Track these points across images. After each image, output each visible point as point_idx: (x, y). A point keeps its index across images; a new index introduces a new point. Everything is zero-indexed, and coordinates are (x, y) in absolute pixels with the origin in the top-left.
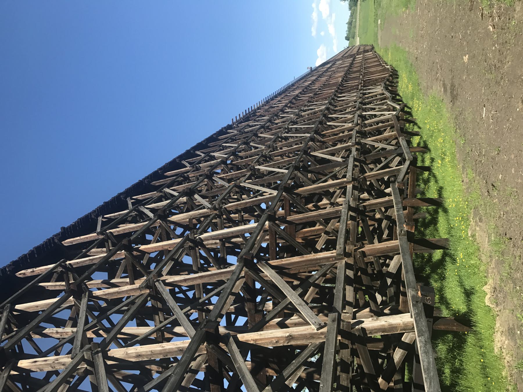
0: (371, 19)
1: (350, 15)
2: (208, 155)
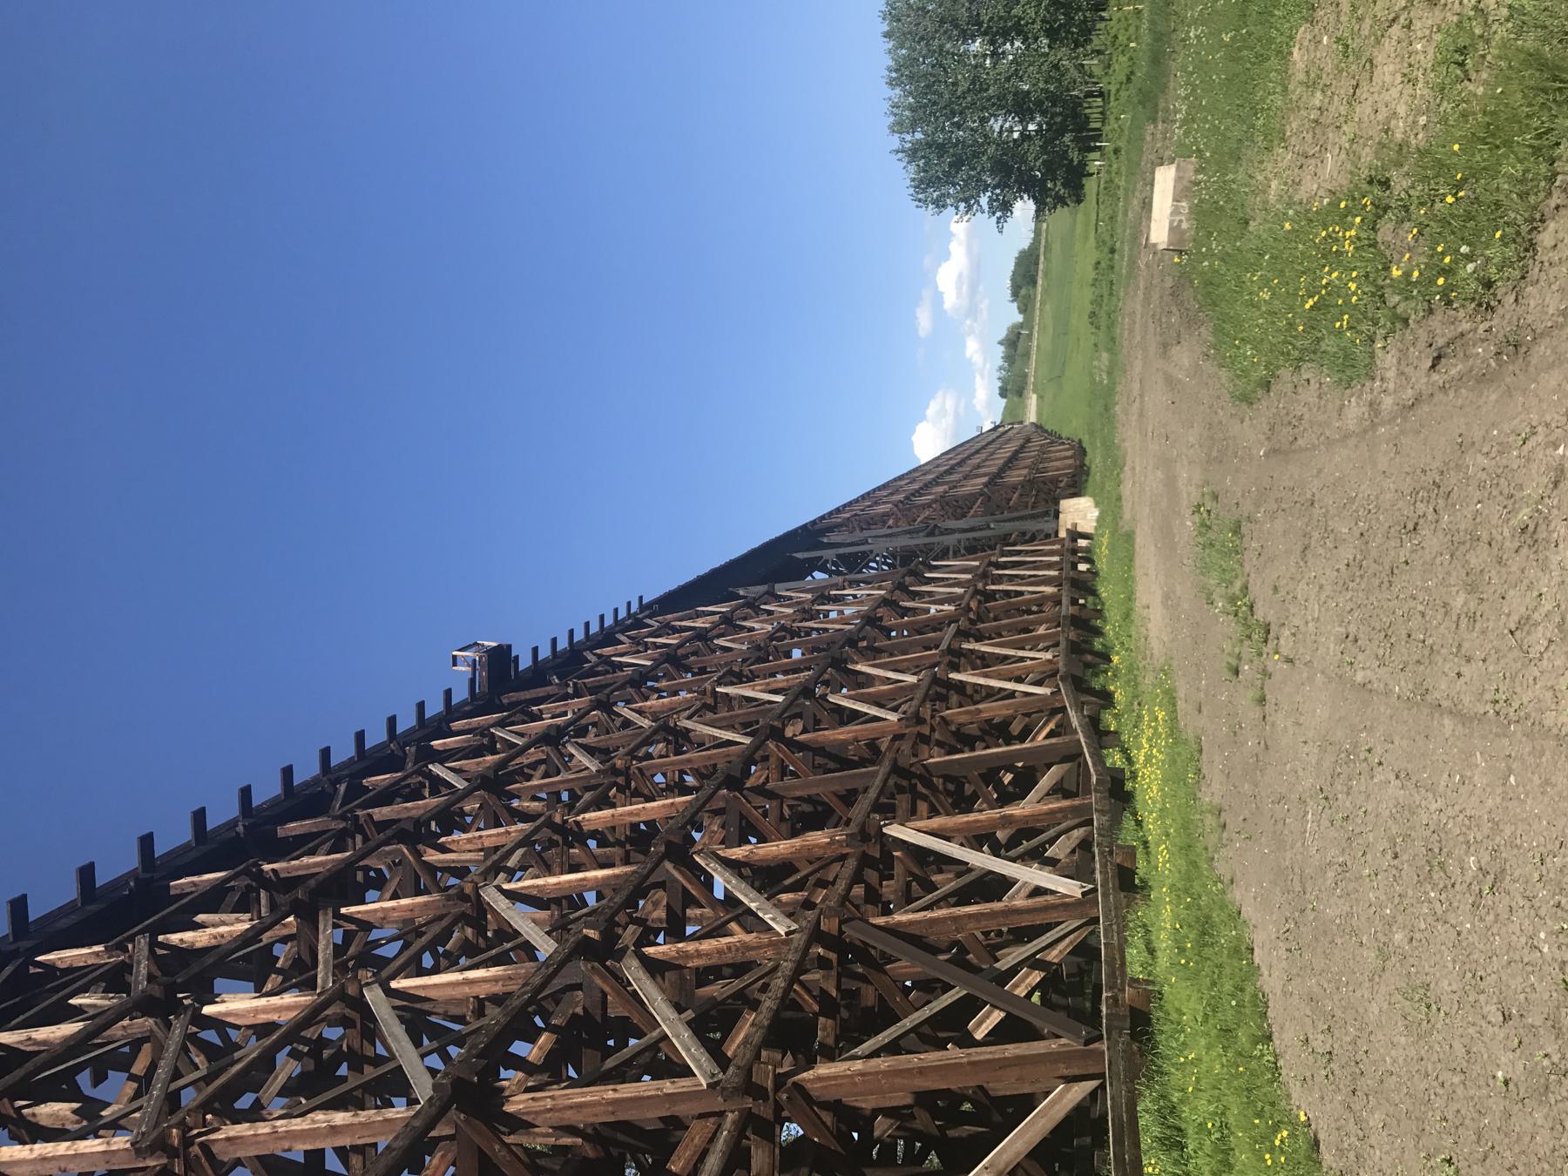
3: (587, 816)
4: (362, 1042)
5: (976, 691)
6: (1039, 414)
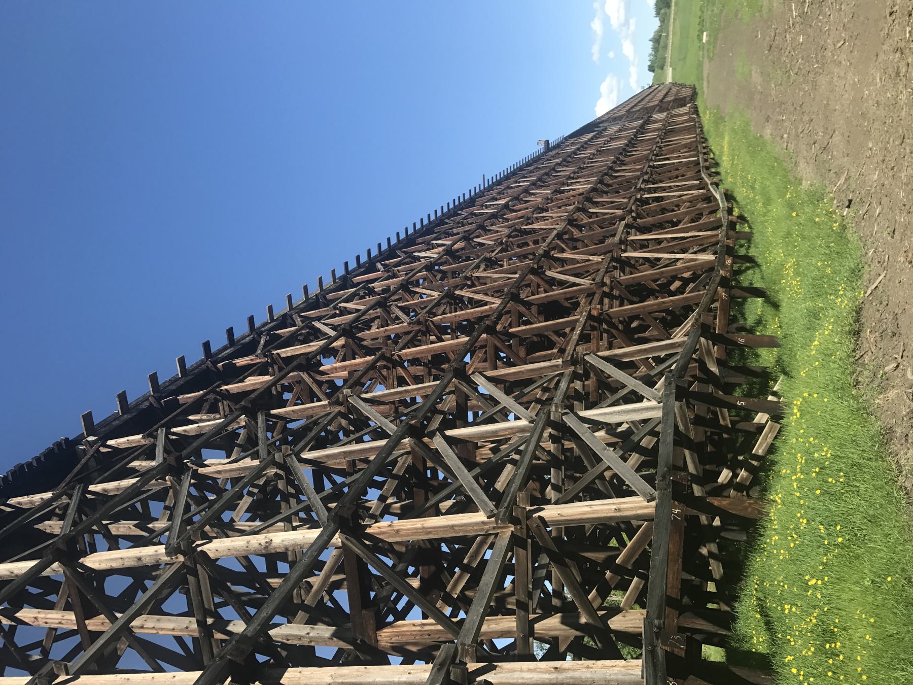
0: (694, 33)
3: (404, 351)
4: (287, 487)
5: (637, 261)
6: (673, 78)
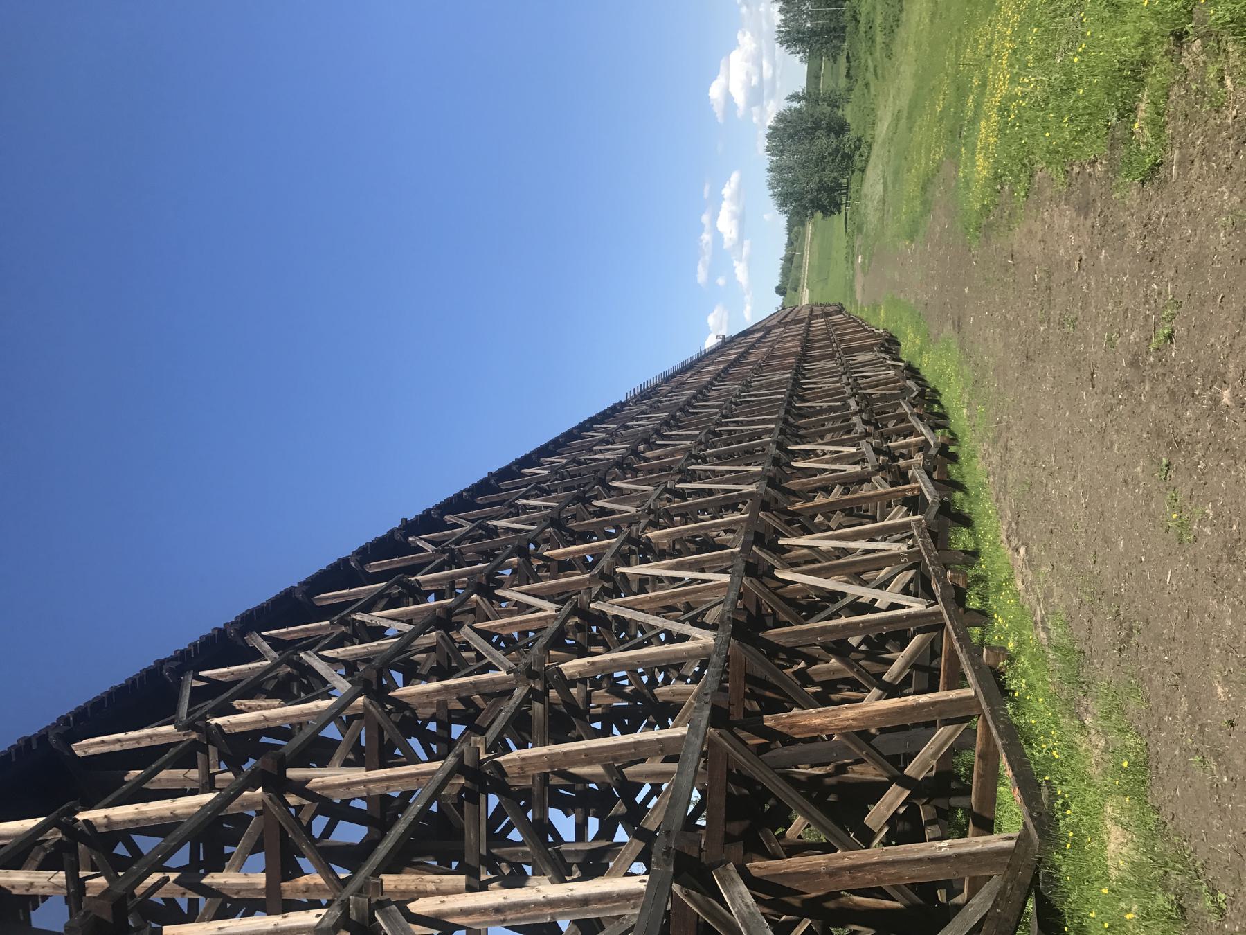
1: (786, 242)
2: (480, 527)
6: (810, 299)
